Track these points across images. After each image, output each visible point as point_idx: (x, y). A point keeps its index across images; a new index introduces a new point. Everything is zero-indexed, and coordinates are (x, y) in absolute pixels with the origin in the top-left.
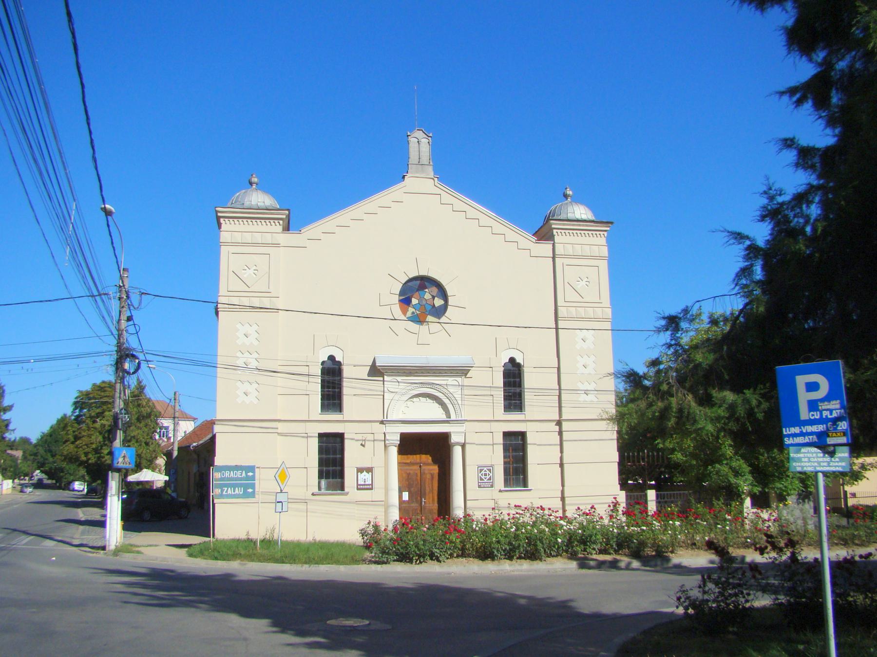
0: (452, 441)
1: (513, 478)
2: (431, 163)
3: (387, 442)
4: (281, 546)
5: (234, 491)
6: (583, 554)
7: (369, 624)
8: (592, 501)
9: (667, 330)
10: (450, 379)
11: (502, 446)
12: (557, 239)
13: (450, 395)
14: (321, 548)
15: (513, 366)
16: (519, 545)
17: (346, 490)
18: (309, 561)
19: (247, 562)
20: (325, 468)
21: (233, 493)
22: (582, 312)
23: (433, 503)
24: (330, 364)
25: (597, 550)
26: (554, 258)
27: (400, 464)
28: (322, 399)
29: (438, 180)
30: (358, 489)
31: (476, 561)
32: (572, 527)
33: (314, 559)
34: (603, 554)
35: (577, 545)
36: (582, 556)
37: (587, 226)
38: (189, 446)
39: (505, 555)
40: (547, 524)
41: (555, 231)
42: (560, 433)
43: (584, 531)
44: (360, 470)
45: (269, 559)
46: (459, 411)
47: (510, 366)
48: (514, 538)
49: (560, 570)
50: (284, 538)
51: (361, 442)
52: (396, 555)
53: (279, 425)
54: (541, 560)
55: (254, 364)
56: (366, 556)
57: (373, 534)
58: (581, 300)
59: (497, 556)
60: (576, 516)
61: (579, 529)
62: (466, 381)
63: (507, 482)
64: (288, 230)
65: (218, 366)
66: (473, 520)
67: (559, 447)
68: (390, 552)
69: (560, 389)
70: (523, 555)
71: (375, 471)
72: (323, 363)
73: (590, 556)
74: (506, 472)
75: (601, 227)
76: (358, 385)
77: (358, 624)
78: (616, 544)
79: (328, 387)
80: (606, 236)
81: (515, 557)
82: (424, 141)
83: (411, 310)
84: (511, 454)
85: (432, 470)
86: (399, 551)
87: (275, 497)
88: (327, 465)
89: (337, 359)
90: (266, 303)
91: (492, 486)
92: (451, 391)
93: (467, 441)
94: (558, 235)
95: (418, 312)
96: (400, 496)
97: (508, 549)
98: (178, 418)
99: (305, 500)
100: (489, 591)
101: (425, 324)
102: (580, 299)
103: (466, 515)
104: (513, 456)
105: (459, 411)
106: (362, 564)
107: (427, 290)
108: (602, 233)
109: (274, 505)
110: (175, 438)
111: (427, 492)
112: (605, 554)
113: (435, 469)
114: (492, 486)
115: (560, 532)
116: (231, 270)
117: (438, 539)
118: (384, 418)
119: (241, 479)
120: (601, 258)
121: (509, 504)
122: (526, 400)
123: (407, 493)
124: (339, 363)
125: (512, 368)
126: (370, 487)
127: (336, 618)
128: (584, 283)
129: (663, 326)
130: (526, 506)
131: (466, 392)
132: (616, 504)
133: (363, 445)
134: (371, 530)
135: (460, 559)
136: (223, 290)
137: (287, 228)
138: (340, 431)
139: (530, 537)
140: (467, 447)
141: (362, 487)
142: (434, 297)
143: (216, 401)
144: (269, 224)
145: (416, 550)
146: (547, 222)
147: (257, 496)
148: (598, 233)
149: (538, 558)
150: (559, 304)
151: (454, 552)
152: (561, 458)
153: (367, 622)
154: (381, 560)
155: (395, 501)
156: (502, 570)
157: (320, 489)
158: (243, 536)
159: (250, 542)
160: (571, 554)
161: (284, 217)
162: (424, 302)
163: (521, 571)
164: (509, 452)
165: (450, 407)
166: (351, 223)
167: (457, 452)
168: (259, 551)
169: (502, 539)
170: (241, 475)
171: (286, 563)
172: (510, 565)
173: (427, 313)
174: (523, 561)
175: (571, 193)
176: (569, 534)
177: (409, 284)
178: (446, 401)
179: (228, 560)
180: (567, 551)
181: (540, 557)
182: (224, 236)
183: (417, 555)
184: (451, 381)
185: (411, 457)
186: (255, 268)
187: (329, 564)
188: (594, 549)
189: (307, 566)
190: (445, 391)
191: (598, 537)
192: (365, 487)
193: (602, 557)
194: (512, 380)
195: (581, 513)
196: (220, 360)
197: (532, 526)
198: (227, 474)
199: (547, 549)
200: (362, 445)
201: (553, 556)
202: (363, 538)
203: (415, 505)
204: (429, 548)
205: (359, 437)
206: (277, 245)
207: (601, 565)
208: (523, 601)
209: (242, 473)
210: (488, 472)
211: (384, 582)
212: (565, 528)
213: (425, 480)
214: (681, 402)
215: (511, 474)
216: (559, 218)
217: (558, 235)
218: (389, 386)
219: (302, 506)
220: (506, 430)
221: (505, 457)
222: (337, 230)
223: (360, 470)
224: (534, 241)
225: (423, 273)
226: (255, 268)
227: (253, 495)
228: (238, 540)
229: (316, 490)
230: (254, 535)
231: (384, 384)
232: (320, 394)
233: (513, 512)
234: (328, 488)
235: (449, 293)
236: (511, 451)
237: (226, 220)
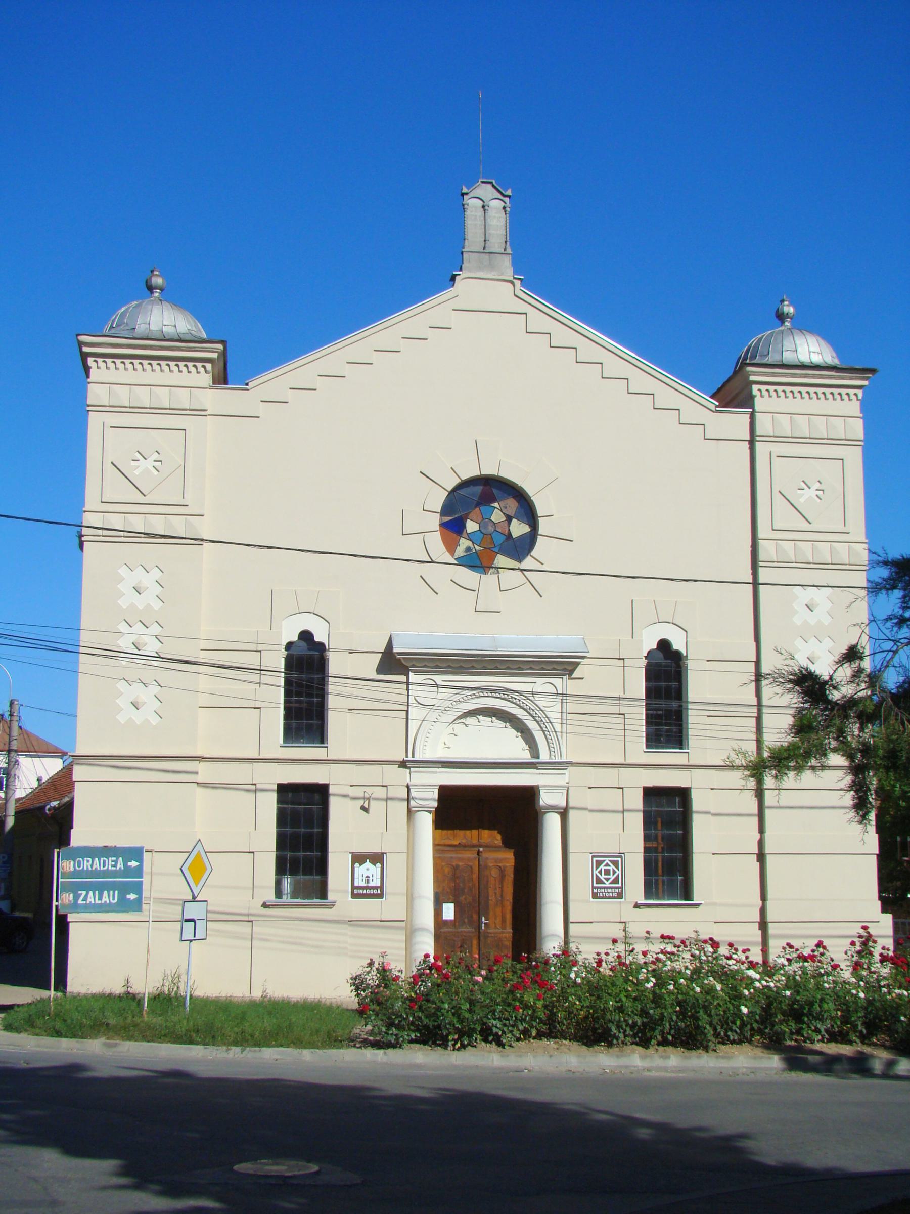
0: (541, 803)
1: (663, 881)
2: (509, 251)
3: (412, 803)
4: (192, 1009)
5: (100, 898)
6: (796, 1040)
7: (317, 1173)
8: (820, 931)
9: (894, 587)
10: (540, 681)
11: (641, 815)
12: (759, 404)
13: (540, 714)
14: (270, 1013)
16: (662, 1017)
17: (331, 896)
18: (243, 1040)
19: (118, 1041)
21: (98, 902)
23: (504, 927)
24: (303, 648)
25: (823, 1032)
26: (752, 442)
27: (439, 848)
29: (522, 286)
30: (354, 896)
31: (575, 1045)
32: (772, 985)
33: (252, 1036)
35: (781, 1022)
36: (793, 1043)
37: (822, 377)
39: (635, 1036)
40: (723, 975)
41: (755, 388)
43: (798, 993)
44: (359, 859)
45: (165, 1035)
46: (556, 744)
47: (660, 658)
49: (744, 1070)
51: (361, 803)
52: (414, 1031)
53: (200, 767)
54: (706, 1049)
55: (152, 647)
57: (378, 986)
59: (617, 1038)
61: (787, 987)
63: (650, 889)
64: (226, 383)
65: (82, 650)
67: (755, 820)
68: (403, 1023)
69: (759, 705)
70: (670, 1038)
71: (389, 860)
72: (289, 646)
73: (808, 1045)
74: (649, 868)
75: (851, 379)
77: (296, 1173)
79: (299, 694)
81: (653, 1042)
82: (496, 205)
83: (464, 543)
85: (501, 860)
89: (317, 639)
90: (178, 526)
91: (620, 896)
92: (541, 704)
93: (571, 805)
94: (762, 396)
95: (478, 548)
96: (438, 912)
97: (639, 1023)
98: (16, 751)
99: (249, 915)
100: (583, 1110)
101: (491, 570)
102: (804, 526)
104: (663, 838)
105: (556, 744)
107: (496, 505)
108: (852, 392)
110: (11, 792)
111: (491, 903)
113: (508, 858)
114: (620, 896)
115: (746, 992)
116: (109, 459)
117: (499, 1000)
118: (407, 756)
119: (115, 874)
120: (848, 442)
121: (648, 932)
122: (690, 726)
123: (452, 906)
124: (321, 645)
126: (377, 893)
127: (254, 1159)
128: (812, 493)
129: (884, 580)
130: (684, 937)
131: (571, 707)
132: (867, 940)
133: (365, 809)
134: (372, 979)
135: (545, 1042)
136: (92, 500)
137: (222, 378)
139: (685, 1001)
140: (572, 815)
141: (361, 891)
142: (509, 519)
143: (76, 716)
144: (184, 369)
145: (455, 1020)
147: (144, 907)
150: (761, 534)
151: (532, 1027)
153: (315, 1168)
154: (384, 1040)
155: (426, 918)
156: (627, 1067)
157: (279, 893)
158: (118, 989)
160: (771, 1039)
162: (491, 529)
163: (665, 1069)
164: (656, 829)
165: (538, 736)
166: (348, 370)
167: (552, 824)
168: (146, 1019)
169: (628, 1004)
170: (115, 866)
171: (197, 1043)
172: (643, 1057)
173: (496, 550)
174: (670, 1049)
175: (791, 310)
177: (462, 492)
178: (532, 725)
180: (761, 1032)
181: (705, 1043)
182: (96, 393)
183: (457, 1031)
184: (540, 684)
185: (460, 833)
186: (156, 457)
187: (282, 1046)
188: (817, 1031)
189: (237, 1049)
192: (368, 891)
193: (832, 1049)
194: (663, 684)
195: (795, 955)
196: (86, 638)
197: (691, 979)
199: (719, 1028)
200: (363, 808)
201: (733, 1042)
202: (358, 995)
203: (467, 929)
205: (358, 792)
206: (200, 412)
207: (829, 1065)
208: (643, 1133)
209: (116, 862)
210: (612, 867)
211: (376, 1085)
212: (757, 984)
213: (488, 882)
214: (894, 737)
215: (660, 871)
216: (765, 361)
217: (762, 396)
218: (419, 694)
219: (245, 929)
220: (650, 784)
221: (647, 838)
223: (359, 859)
225: (489, 470)
227: (137, 906)
228: (110, 995)
229: (271, 896)
231: (408, 689)
232: (282, 706)
233: (655, 948)
235: (540, 511)
236: (659, 825)
237: (100, 360)
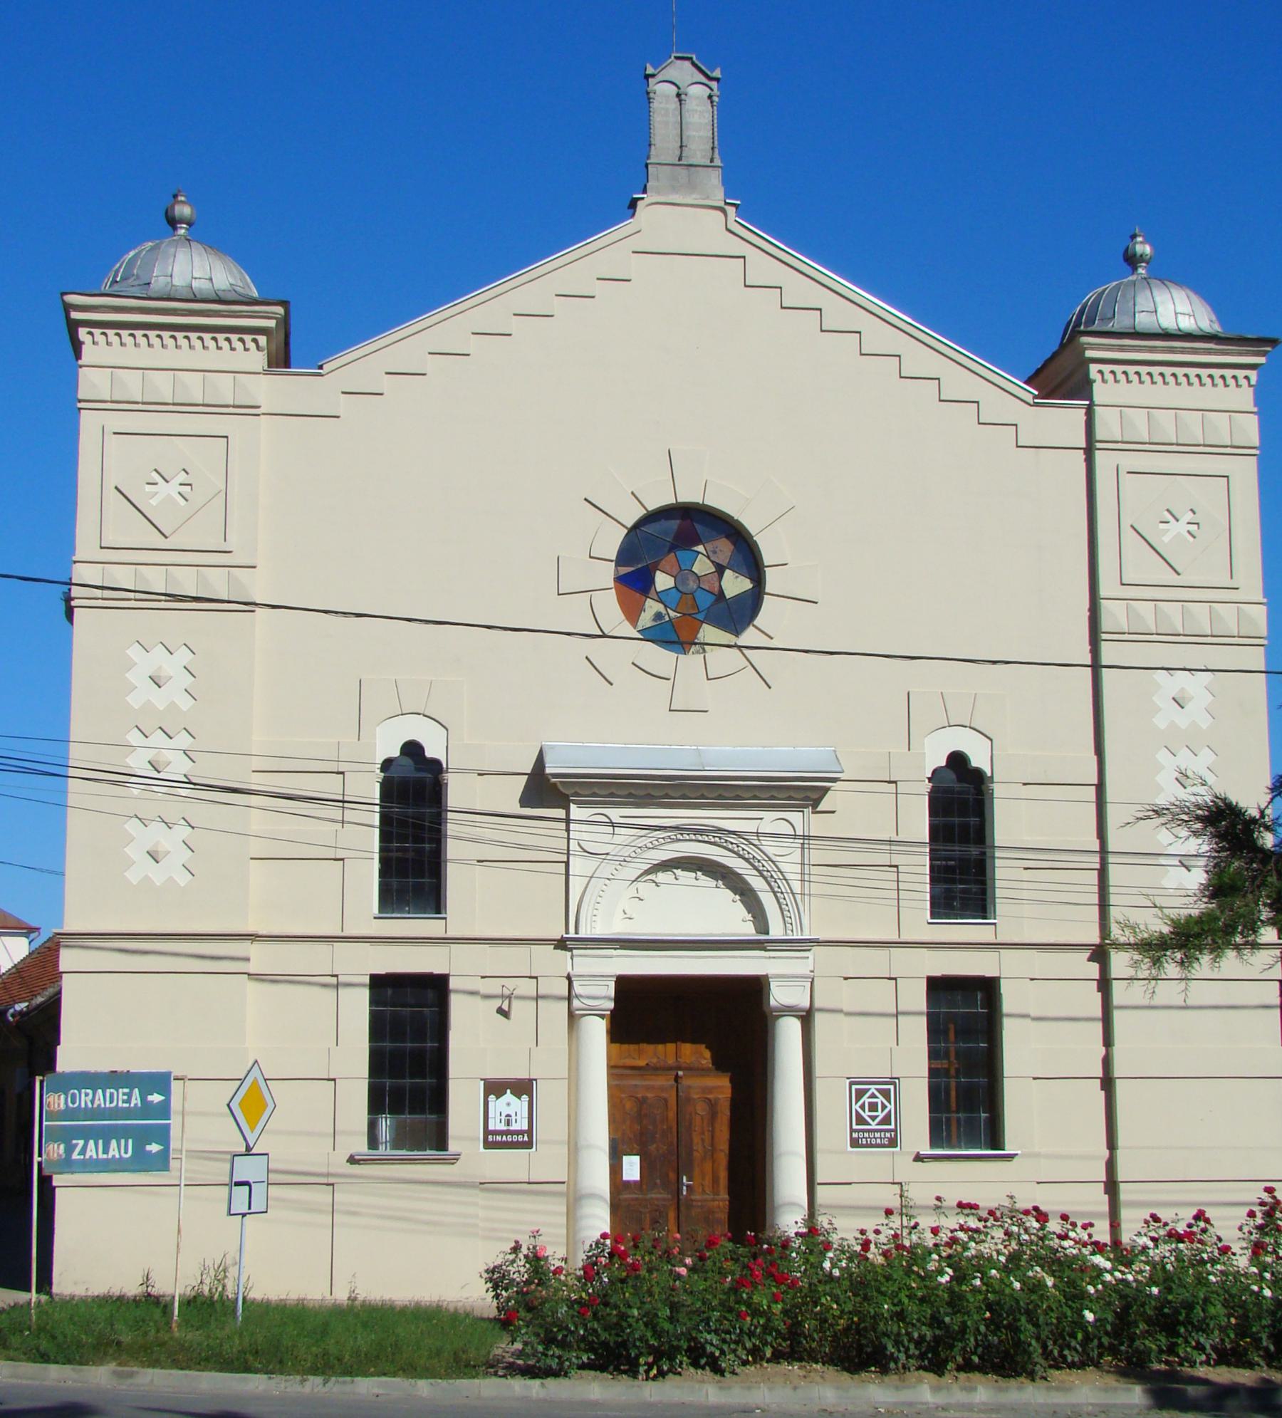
0: (772, 1002)
1: (958, 1120)
2: (718, 162)
3: (576, 1003)
4: (246, 1319)
5: (106, 1151)
6: (1167, 1362)
8: (1200, 1195)
10: (769, 816)
12: (1100, 392)
13: (769, 866)
14: (365, 1325)
15: (960, 779)
16: (964, 1329)
17: (453, 1146)
18: (326, 1366)
19: (135, 1369)
20: (388, 1082)
22: (1174, 616)
24: (408, 769)
26: (1089, 452)
27: (616, 1071)
28: (383, 873)
30: (488, 1145)
31: (831, 1371)
32: (1130, 1277)
34: (1229, 1364)
36: (1163, 1367)
38: (6, 1011)
39: (922, 1356)
40: (1055, 1262)
41: (1094, 368)
42: (1104, 984)
43: (1170, 1290)
44: (495, 1088)
45: (207, 1359)
47: (951, 778)
48: (949, 1304)
50: (256, 1294)
51: (497, 1003)
52: (586, 1351)
54: (1032, 1376)
55: (178, 767)
56: (499, 1352)
57: (527, 1283)
58: (1174, 579)
60: (1144, 1240)
62: (817, 824)
63: (938, 1133)
64: (287, 365)
65: (72, 772)
66: (828, 1246)
67: (1098, 1027)
68: (570, 1338)
69: (1103, 851)
70: (976, 1359)
71: (540, 1090)
72: (387, 764)
73: (1186, 1369)
75: (1240, 354)
76: (488, 834)
78: (1271, 1336)
80: (1253, 382)
81: (950, 1366)
82: (698, 92)
84: (952, 1047)
86: (598, 1336)
87: (228, 1166)
88: (396, 1072)
90: (217, 584)
91: (893, 1143)
92: (770, 851)
93: (817, 1004)
94: (1104, 381)
95: (673, 614)
96: (616, 1169)
99: (328, 1175)
101: (693, 648)
102: (1169, 577)
103: (812, 1230)
106: (486, 1374)
107: (700, 548)
108: (1240, 373)
109: (227, 1188)
112: (1237, 1366)
113: (721, 1086)
114: (893, 1143)
115: (1091, 1289)
116: (109, 485)
118: (567, 932)
120: (1235, 450)
121: (938, 1199)
122: (998, 884)
123: (636, 1159)
124: (436, 763)
125: (957, 786)
126: (523, 1141)
130: (993, 1205)
131: (816, 856)
134: (519, 1271)
135: (785, 1366)
136: (85, 546)
137: (281, 359)
138: (437, 970)
139: (998, 1303)
140: (819, 1020)
142: (720, 570)
143: (63, 874)
144: (225, 345)
145: (649, 1334)
146: (1070, 340)
147: (173, 1164)
148: (1228, 373)
149: (1024, 1370)
150: (1103, 592)
152: (1107, 1062)
154: (541, 1364)
156: (910, 1404)
157: (373, 1142)
158: (132, 1288)
159: (152, 1303)
160: (1129, 1360)
161: (271, 323)
162: (692, 585)
164: (946, 1041)
165: (767, 900)
167: (788, 1034)
169: (911, 1307)
170: (128, 1101)
171: (256, 1371)
172: (936, 1389)
173: (701, 617)
174: (976, 1376)
175: (1147, 249)
176: (1123, 1297)
178: (757, 883)
179: (81, 1364)
180: (1113, 1350)
182: (92, 382)
184: (770, 821)
185: (649, 1048)
186: (182, 477)
187: (385, 1374)
188: (1200, 1348)
190: (754, 852)
191: (1212, 1310)
192: (509, 1138)
193: (1224, 1375)
195: (1162, 1232)
196: (78, 755)
197: (1005, 1269)
198: (85, 1098)
199: (1050, 1343)
200: (500, 1011)
201: (1072, 1366)
202: (497, 1296)
203: (659, 1195)
204: (689, 1330)
205: (493, 987)
206: (249, 410)
209: (130, 1095)
212: (1108, 1277)
215: (953, 1104)
216: (1109, 327)
217: (1104, 381)
218: (585, 836)
219: (321, 1196)
220: (938, 972)
221: (933, 1054)
222: (432, 364)
223: (495, 1088)
224: (1029, 398)
225: (689, 495)
226: (182, 477)
227: (162, 1161)
229: (361, 1146)
230: (164, 1286)
231: (568, 830)
232: (377, 857)
233: (950, 1222)
234: (397, 1143)
237: (97, 332)
